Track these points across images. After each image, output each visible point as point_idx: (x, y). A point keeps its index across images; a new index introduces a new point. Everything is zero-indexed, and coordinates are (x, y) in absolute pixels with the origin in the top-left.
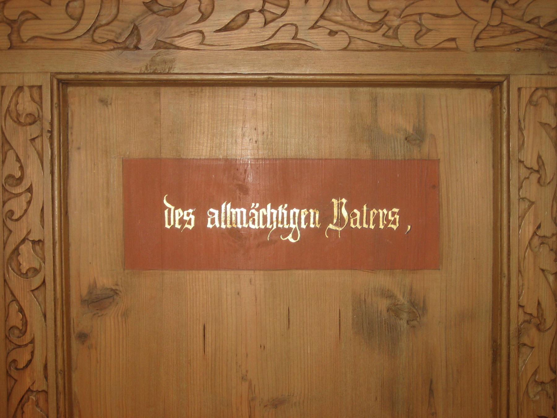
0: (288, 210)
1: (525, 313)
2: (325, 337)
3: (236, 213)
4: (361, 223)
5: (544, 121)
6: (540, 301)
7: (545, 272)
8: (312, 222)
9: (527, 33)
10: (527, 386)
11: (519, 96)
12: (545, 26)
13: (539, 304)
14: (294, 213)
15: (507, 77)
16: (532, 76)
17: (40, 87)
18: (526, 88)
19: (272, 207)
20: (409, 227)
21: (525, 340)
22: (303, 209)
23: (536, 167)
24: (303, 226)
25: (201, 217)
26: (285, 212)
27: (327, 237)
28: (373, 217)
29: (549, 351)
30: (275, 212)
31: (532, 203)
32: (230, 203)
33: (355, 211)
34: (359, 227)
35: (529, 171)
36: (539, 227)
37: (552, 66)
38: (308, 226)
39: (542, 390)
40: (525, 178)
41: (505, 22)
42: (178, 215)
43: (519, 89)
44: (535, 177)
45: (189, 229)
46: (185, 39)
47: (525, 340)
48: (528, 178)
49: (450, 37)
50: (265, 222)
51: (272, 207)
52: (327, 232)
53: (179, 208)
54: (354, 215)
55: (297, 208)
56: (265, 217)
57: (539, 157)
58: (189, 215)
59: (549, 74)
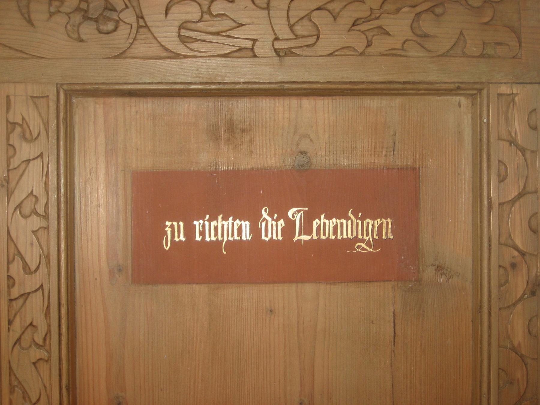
8: (264, 236)
17: (499, 139)
19: (325, 218)
20: (360, 214)
22: (365, 219)
24: (376, 237)
26: (360, 222)
27: (225, 253)
28: (237, 226)
30: (327, 221)
32: (324, 214)
42: (280, 226)
45: (244, 240)
51: (325, 218)
52: (224, 250)
53: (285, 224)
56: (216, 228)
58: (246, 225)
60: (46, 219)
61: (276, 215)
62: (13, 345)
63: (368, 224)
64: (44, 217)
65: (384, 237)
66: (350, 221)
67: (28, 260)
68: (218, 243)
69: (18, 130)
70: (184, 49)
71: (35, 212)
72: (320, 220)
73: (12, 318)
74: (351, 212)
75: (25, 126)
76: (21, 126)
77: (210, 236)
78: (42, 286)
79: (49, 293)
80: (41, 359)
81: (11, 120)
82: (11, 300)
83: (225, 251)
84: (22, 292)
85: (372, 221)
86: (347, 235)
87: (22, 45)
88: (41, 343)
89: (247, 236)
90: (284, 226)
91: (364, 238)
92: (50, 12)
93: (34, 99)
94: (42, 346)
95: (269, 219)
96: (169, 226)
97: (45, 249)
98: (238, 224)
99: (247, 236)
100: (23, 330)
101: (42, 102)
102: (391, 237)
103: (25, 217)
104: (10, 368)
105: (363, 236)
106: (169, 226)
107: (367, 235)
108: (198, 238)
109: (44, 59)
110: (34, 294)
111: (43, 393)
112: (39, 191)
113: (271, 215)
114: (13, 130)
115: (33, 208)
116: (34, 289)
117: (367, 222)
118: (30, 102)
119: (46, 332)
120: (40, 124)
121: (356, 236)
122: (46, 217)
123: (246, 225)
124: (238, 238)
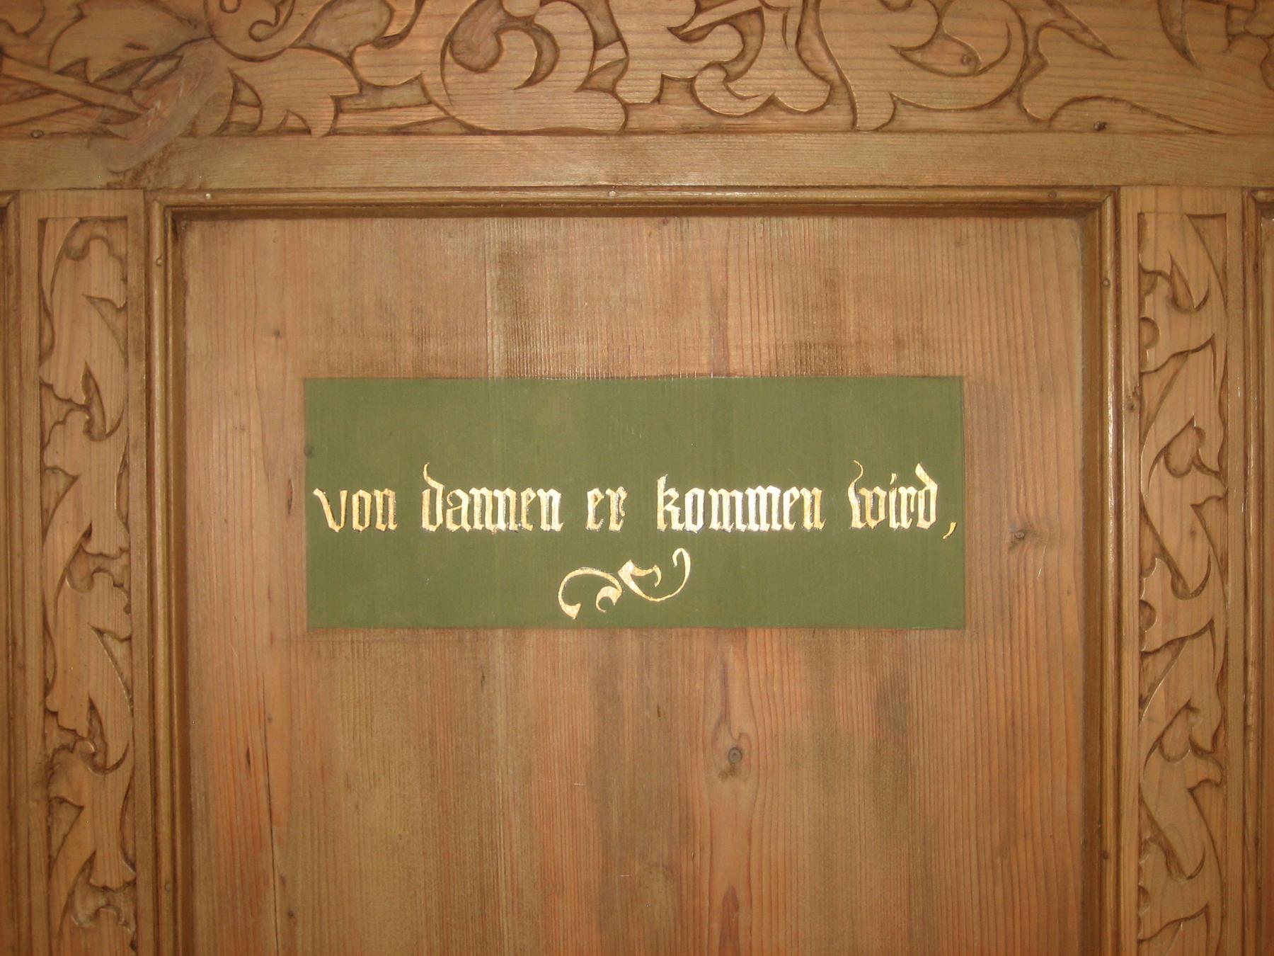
1: (61, 728)
2: (925, 778)
4: (471, 521)
5: (94, 294)
6: (94, 700)
7: (105, 635)
9: (57, 96)
10: (71, 894)
11: (41, 240)
12: (97, 80)
13: (92, 707)
14: (695, 521)
15: (1115, 192)
16: (69, 193)
18: (56, 219)
21: (61, 788)
23: (81, 399)
25: (835, 510)
29: (118, 818)
31: (74, 479)
34: (467, 528)
35: (65, 408)
36: (88, 535)
37: (114, 168)
38: (520, 528)
39: (108, 905)
40: (57, 423)
41: (9, 73)
42: (789, 500)
43: (43, 223)
44: (79, 419)
47: (61, 788)
48: (63, 422)
54: (457, 501)
55: (700, 487)
57: (88, 375)
58: (811, 496)
59: (109, 187)
60: (1219, 479)
62: (1148, 750)
63: (361, 500)
64: (1216, 474)
65: (807, 524)
66: (922, 493)
67: (1183, 568)
69: (1163, 287)
71: (1198, 464)
73: (1146, 694)
74: (429, 474)
75: (1177, 280)
76: (1169, 279)
77: (550, 522)
78: (1211, 622)
79: (1226, 637)
80: (1207, 781)
81: (1149, 266)
82: (1144, 655)
84: (1170, 637)
85: (885, 493)
86: (812, 520)
87: (1170, 104)
88: (1208, 747)
89: (813, 521)
92: (1228, 35)
93: (1199, 222)
94: (1209, 753)
96: (672, 502)
97: (1218, 542)
99: (813, 521)
100: (1170, 718)
101: (1213, 225)
102: (597, 527)
103: (1174, 473)
104: (1141, 801)
105: (771, 524)
106: (672, 502)
108: (591, 524)
109: (1217, 135)
110: (1196, 641)
111: (1210, 852)
112: (1208, 420)
114: (1153, 286)
115: (1195, 451)
116: (1195, 631)
117: (359, 497)
118: (1190, 229)
119: (1219, 720)
120: (1209, 275)
121: (370, 525)
122: (1220, 474)
123: (551, 498)
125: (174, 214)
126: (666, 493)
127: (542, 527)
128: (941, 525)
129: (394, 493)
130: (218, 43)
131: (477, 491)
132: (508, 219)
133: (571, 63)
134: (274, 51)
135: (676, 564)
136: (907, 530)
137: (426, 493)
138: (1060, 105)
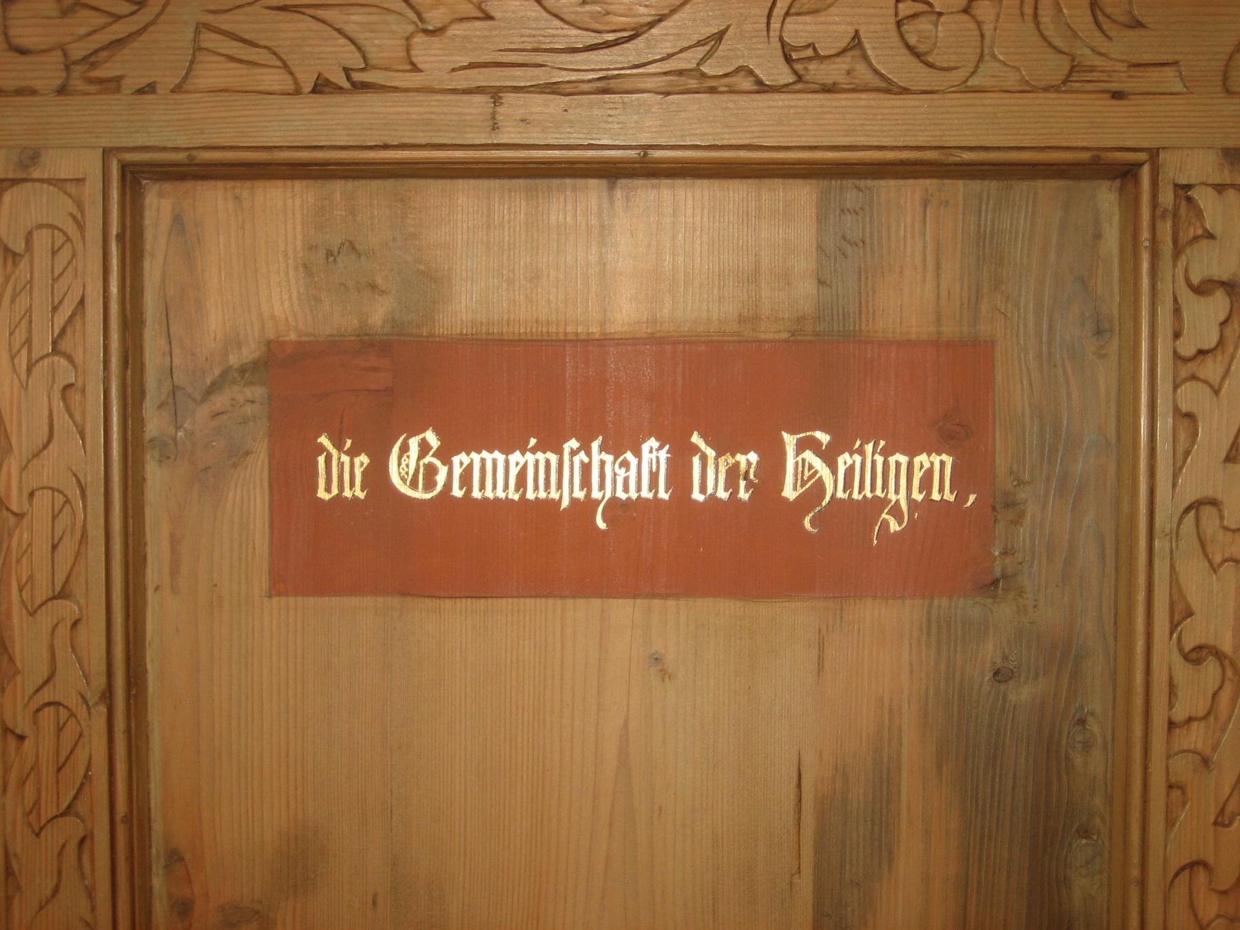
0: (886, 453)
3: (537, 461)
14: (898, 464)
19: (603, 448)
20: (972, 498)
24: (918, 497)
26: (879, 459)
27: (601, 524)
32: (562, 508)
33: (629, 456)
34: (869, 495)
42: (459, 466)
46: (435, 98)
49: (23, 59)
50: (586, 483)
51: (603, 448)
54: (625, 464)
55: (904, 453)
61: (349, 443)
68: (589, 505)
70: (344, 46)
72: (589, 454)
83: (605, 520)
90: (368, 465)
91: (889, 496)
95: (334, 452)
98: (922, 467)
107: (897, 491)
113: (339, 446)
124: (650, 496)
125: (124, 168)
126: (798, 459)
127: (319, 495)
128: (961, 499)
129: (807, 451)
130: (958, 12)
131: (744, 456)
132: (780, 180)
133: (654, 13)
134: (226, 8)
135: (969, 504)
136: (701, 503)
137: (321, 460)
138: (151, 28)
